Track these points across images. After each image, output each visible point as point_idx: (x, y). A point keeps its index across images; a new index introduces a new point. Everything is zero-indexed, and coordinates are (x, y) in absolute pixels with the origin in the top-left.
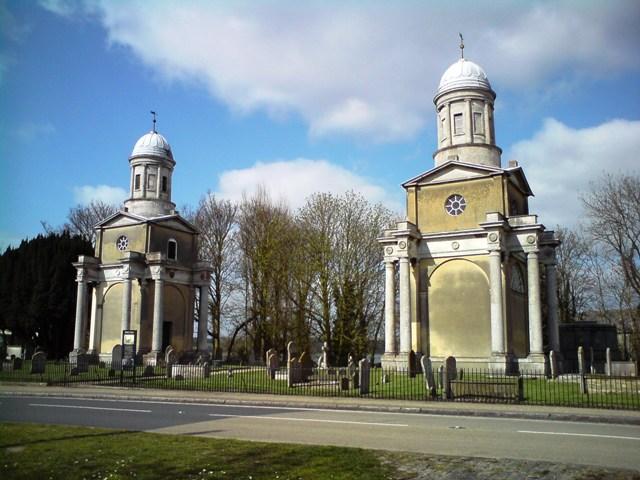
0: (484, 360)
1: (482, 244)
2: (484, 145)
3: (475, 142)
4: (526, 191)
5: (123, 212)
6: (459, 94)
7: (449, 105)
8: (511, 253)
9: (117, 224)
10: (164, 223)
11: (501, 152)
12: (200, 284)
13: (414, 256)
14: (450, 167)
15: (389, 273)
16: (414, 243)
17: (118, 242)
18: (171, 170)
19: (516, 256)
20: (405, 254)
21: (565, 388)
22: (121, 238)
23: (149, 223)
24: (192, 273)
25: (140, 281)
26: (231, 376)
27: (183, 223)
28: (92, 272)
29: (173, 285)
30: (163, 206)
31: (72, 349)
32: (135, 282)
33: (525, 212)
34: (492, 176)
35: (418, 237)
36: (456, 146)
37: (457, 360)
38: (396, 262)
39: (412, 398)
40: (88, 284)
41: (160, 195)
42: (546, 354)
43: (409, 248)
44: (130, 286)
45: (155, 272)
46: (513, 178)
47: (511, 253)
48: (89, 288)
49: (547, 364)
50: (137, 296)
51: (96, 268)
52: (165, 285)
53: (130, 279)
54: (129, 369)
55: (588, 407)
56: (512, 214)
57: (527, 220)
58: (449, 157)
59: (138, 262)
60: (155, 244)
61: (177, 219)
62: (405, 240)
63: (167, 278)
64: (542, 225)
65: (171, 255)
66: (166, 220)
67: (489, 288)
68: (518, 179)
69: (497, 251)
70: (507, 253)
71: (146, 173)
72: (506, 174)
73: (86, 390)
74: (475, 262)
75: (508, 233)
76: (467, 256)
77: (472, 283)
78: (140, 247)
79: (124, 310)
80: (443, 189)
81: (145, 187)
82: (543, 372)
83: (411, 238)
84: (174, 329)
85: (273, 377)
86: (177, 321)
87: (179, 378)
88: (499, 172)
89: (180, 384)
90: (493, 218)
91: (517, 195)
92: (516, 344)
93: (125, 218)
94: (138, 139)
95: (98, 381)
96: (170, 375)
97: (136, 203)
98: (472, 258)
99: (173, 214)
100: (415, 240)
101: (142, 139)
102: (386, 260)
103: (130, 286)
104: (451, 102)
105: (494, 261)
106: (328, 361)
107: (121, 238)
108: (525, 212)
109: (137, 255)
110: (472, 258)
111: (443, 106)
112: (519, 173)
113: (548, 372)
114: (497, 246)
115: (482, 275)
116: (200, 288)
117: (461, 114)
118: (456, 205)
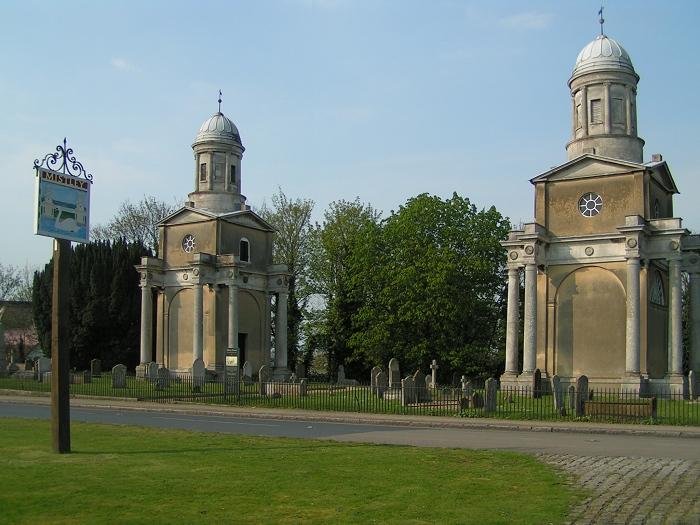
0: (616, 381)
1: (620, 250)
2: (626, 136)
3: (591, 132)
4: (670, 188)
5: (189, 208)
6: (598, 77)
7: (586, 90)
8: (651, 261)
9: (182, 221)
10: (235, 220)
11: (643, 143)
12: (277, 289)
13: (541, 262)
14: (585, 161)
15: (511, 282)
16: (542, 248)
17: (581, 202)
18: (239, 157)
19: (657, 263)
20: (531, 260)
21: (612, 412)
22: (188, 236)
23: (218, 219)
24: (268, 277)
25: (211, 285)
26: (332, 395)
27: (257, 219)
28: (156, 276)
29: (247, 291)
30: (233, 200)
31: (692, 377)
32: (206, 288)
33: (669, 215)
34: (633, 172)
35: (547, 241)
36: (592, 137)
37: (590, 381)
38: (521, 268)
39: (543, 418)
40: (152, 289)
41: (229, 188)
42: (686, 374)
43: (537, 254)
44: (201, 292)
45: (229, 279)
46: (657, 175)
47: (651, 261)
48: (154, 294)
49: (686, 385)
50: (209, 303)
51: (162, 268)
52: (240, 291)
53: (201, 284)
54: (211, 385)
55: (359, 411)
56: (654, 217)
57: (670, 225)
58: (584, 150)
59: (209, 265)
60: (224, 246)
61: (250, 214)
62: (533, 244)
63: (240, 283)
64: (686, 230)
65: (244, 257)
66: (237, 216)
67: (625, 299)
68: (662, 176)
69: (636, 258)
70: (646, 261)
71: (212, 162)
72: (648, 170)
73: (188, 406)
74: (611, 270)
75: (648, 235)
76: (608, 259)
77: (607, 295)
78: (211, 249)
79: (195, 321)
80: (577, 187)
81: (211, 178)
82: (682, 392)
83: (539, 242)
84: (249, 341)
85: (381, 396)
86: (259, 336)
87: (277, 396)
88: (641, 168)
89: (276, 400)
90: (632, 221)
91: (660, 193)
92: (655, 361)
93: (193, 214)
94: (588, 43)
95: (179, 398)
96: (264, 393)
97: (202, 197)
98: (608, 266)
99: (244, 210)
100: (544, 245)
101: (589, 46)
102: (509, 266)
103: (201, 292)
104: (587, 86)
105: (630, 267)
106: (437, 380)
107: (188, 236)
108: (669, 215)
109: (207, 257)
110: (608, 266)
111: (578, 90)
112: (663, 169)
113: (686, 395)
114: (635, 253)
115: (618, 286)
116: (277, 295)
117: (599, 100)
118: (591, 205)
